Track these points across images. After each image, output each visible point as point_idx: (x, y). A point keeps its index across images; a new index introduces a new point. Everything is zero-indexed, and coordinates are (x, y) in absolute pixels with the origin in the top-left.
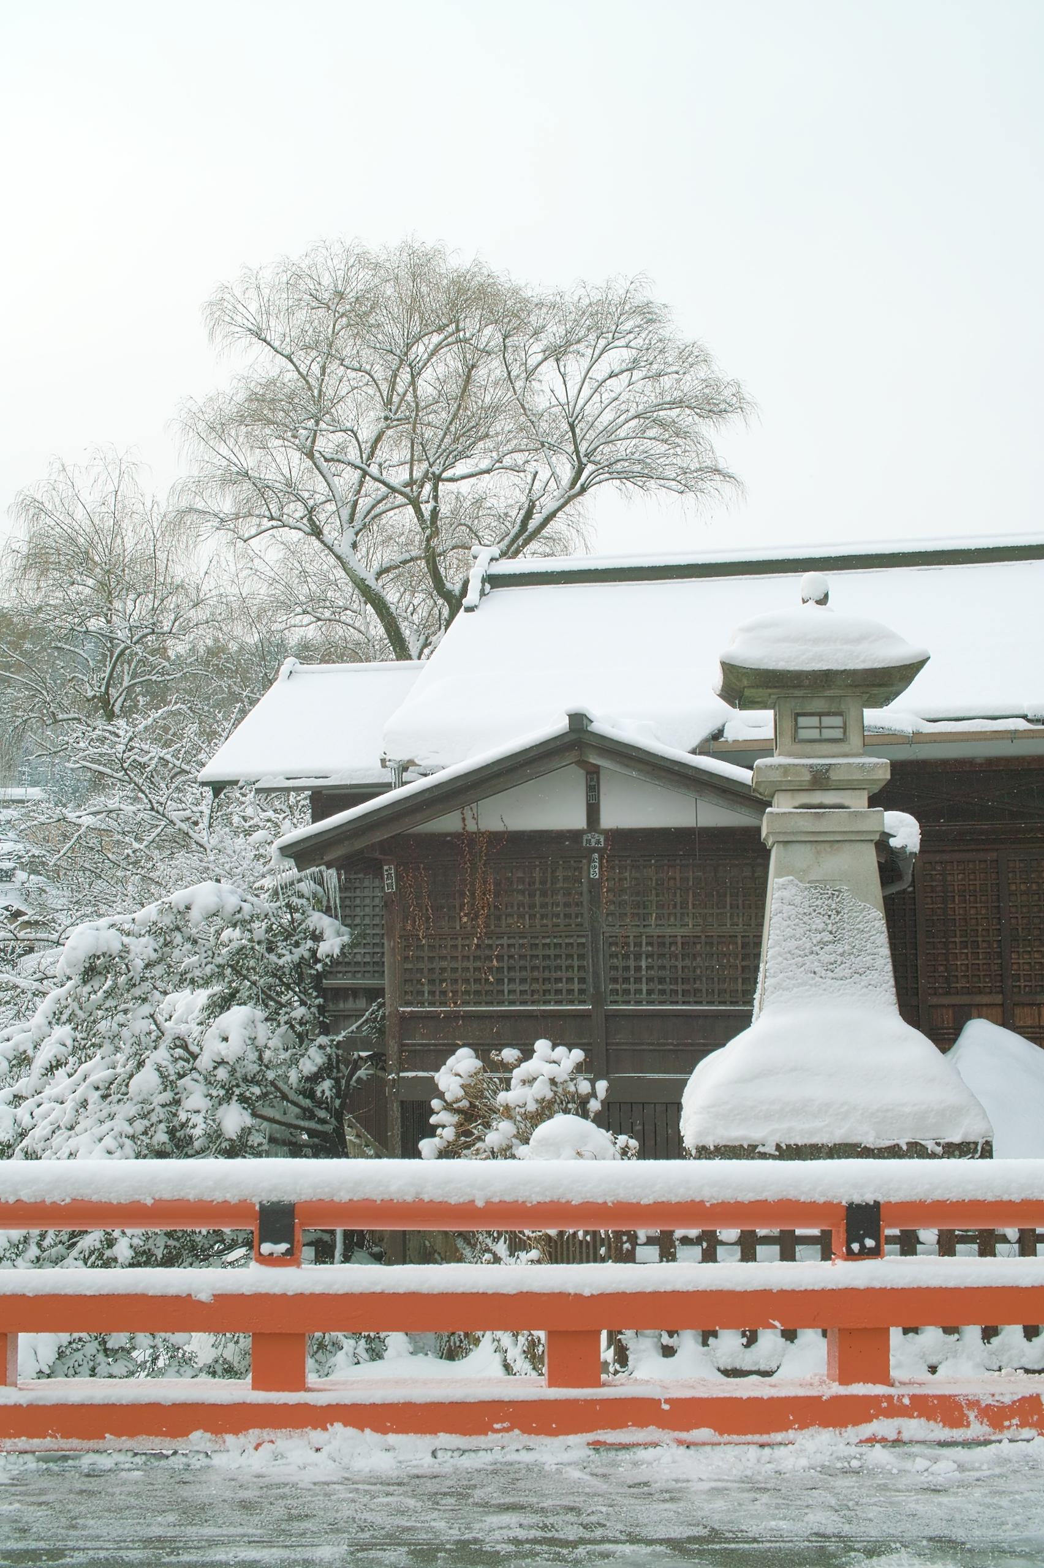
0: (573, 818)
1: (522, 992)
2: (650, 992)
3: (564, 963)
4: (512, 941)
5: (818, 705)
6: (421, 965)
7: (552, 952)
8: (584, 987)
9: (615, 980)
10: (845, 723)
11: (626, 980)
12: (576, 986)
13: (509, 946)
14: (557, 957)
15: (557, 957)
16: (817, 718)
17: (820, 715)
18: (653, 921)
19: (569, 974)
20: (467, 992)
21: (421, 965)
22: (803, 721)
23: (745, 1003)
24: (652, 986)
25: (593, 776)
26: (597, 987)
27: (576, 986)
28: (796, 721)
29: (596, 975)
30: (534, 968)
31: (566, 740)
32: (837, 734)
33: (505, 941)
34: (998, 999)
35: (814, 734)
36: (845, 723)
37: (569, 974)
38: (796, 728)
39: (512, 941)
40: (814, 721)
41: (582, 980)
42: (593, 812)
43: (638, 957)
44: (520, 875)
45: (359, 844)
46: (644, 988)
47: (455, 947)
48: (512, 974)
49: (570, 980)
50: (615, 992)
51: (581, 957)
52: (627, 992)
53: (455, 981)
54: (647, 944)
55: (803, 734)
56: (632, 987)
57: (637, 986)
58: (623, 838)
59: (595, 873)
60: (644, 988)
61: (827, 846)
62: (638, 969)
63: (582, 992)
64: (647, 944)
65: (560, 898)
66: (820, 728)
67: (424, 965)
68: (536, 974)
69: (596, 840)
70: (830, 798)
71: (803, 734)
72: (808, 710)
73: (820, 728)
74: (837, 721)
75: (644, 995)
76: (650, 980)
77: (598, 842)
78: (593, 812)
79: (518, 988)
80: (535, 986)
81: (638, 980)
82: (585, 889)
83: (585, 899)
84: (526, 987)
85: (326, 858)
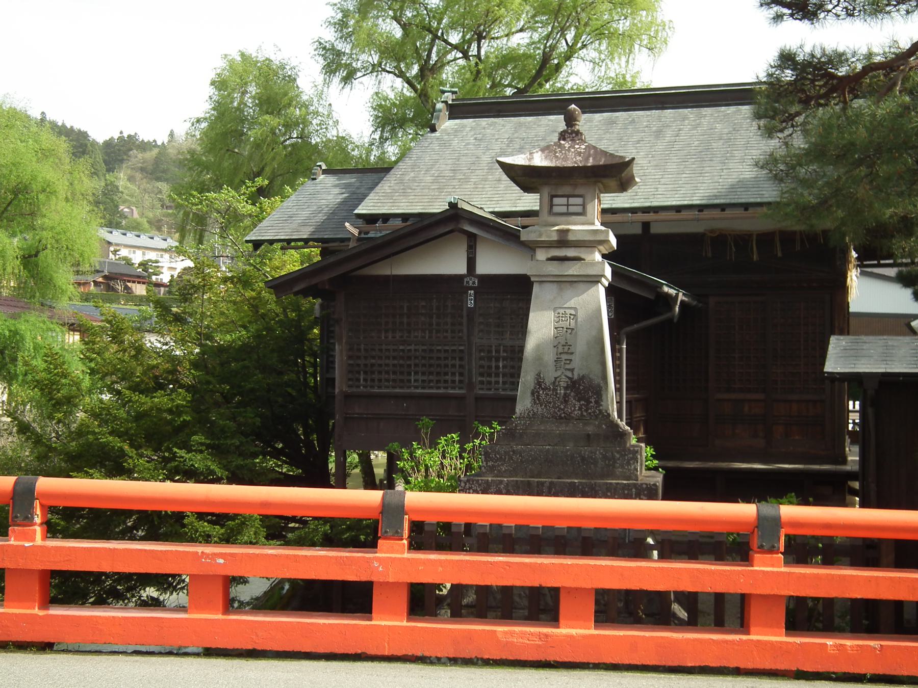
0: (458, 267)
1: (423, 381)
2: (504, 383)
3: (450, 362)
4: (417, 347)
5: (567, 190)
6: (359, 362)
7: (442, 355)
8: (462, 378)
9: (482, 375)
10: (584, 202)
11: (490, 375)
12: (457, 378)
13: (415, 350)
14: (446, 358)
15: (446, 358)
16: (566, 199)
17: (568, 196)
18: (508, 335)
19: (453, 370)
20: (388, 381)
21: (359, 362)
22: (556, 201)
23: (512, 390)
24: (506, 379)
25: (472, 241)
26: (470, 378)
27: (457, 378)
28: (551, 201)
29: (470, 371)
30: (431, 366)
31: (448, 214)
32: (579, 209)
33: (412, 347)
34: (761, 396)
35: (563, 209)
36: (584, 202)
37: (453, 370)
38: (552, 206)
39: (417, 347)
40: (563, 201)
41: (461, 374)
42: (471, 263)
43: (497, 360)
44: (424, 304)
45: (314, 281)
46: (501, 380)
47: (381, 350)
48: (417, 369)
49: (453, 374)
50: (482, 382)
51: (461, 359)
52: (402, 381)
53: (380, 373)
54: (504, 351)
55: (556, 209)
56: (493, 379)
57: (496, 379)
58: (488, 280)
59: (471, 304)
60: (501, 380)
61: (568, 284)
62: (497, 367)
63: (461, 382)
64: (504, 351)
65: (449, 320)
66: (568, 205)
67: (361, 362)
68: (432, 369)
69: (473, 282)
70: (571, 253)
71: (556, 209)
72: (576, 193)
73: (568, 205)
74: (579, 201)
75: (501, 385)
76: (504, 375)
77: (474, 283)
78: (471, 263)
79: (420, 377)
80: (431, 377)
81: (497, 375)
82: (465, 313)
83: (465, 320)
84: (425, 378)
85: (296, 289)
